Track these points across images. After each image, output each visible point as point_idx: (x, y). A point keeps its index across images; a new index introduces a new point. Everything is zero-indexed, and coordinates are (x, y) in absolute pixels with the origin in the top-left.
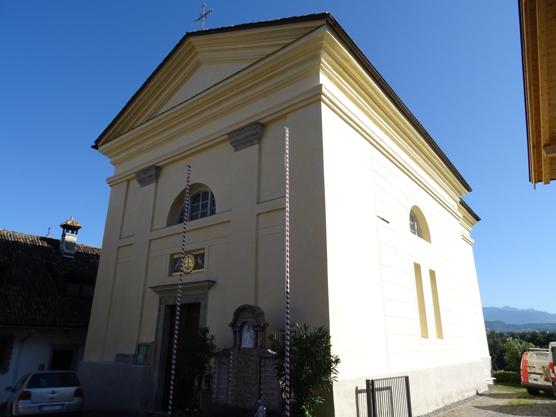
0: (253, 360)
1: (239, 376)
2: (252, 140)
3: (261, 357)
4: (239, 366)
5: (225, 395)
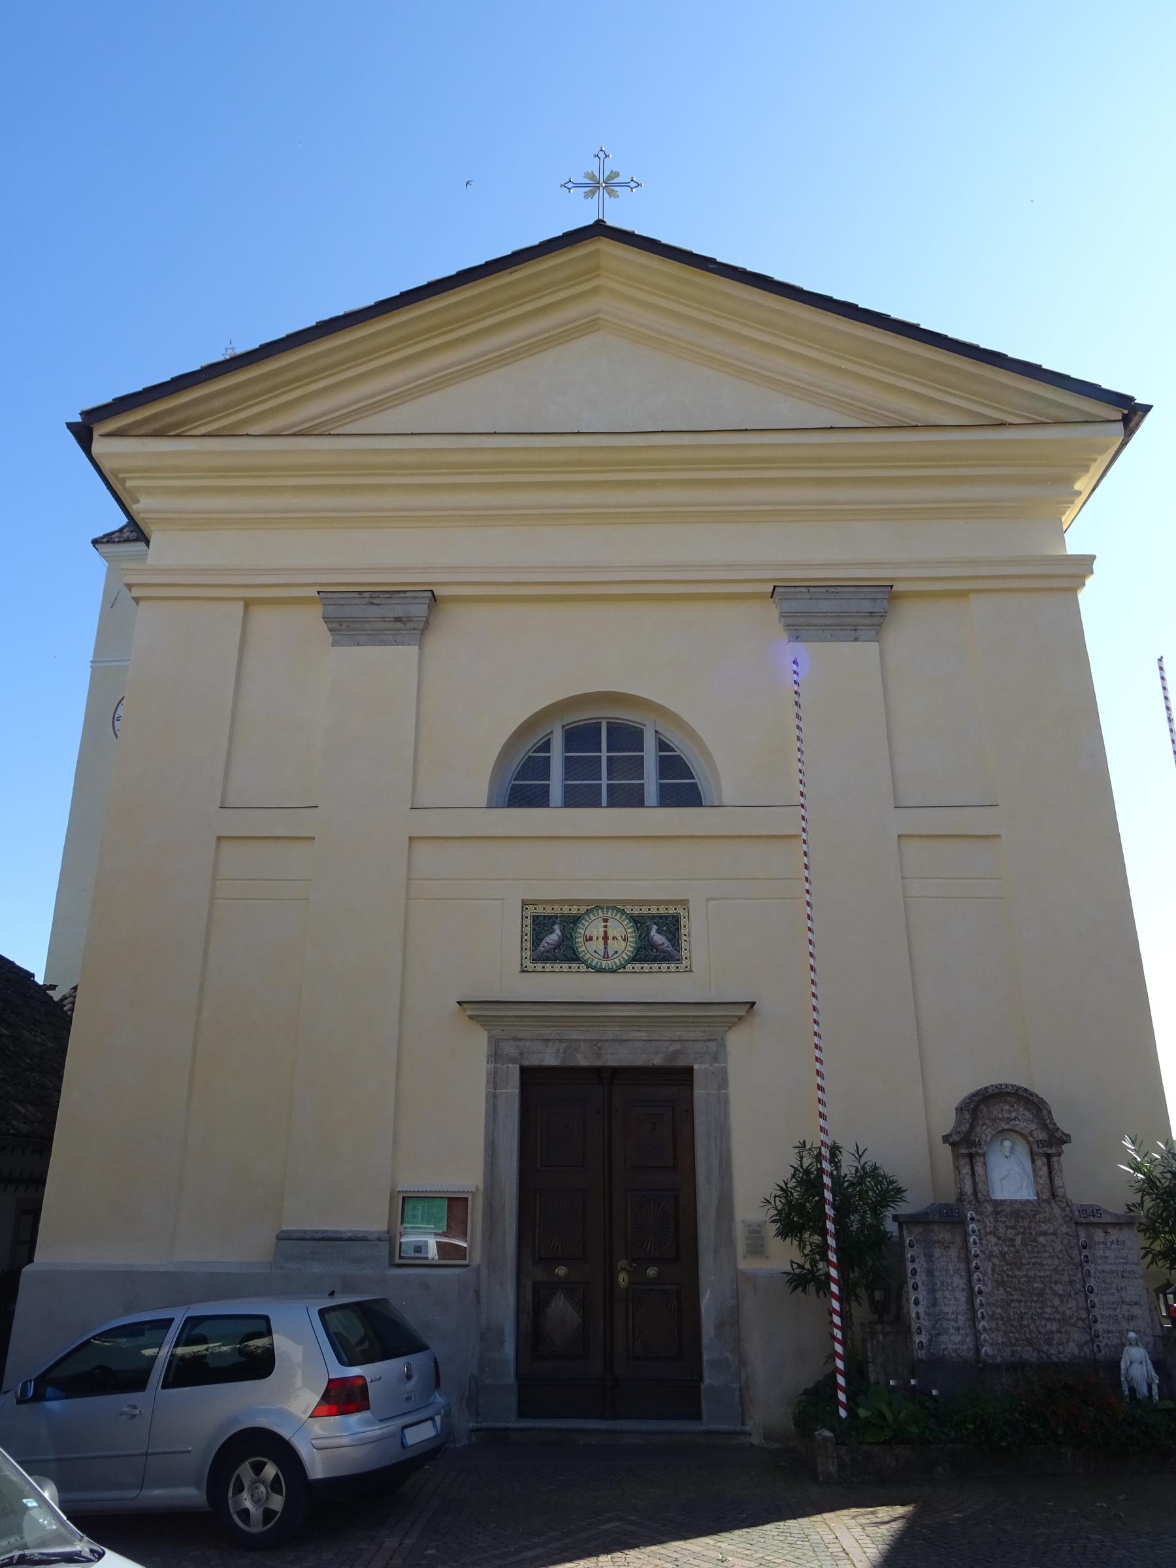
0: (1051, 1231)
1: (1008, 1276)
2: (856, 626)
3: (1077, 1224)
5: (962, 1332)
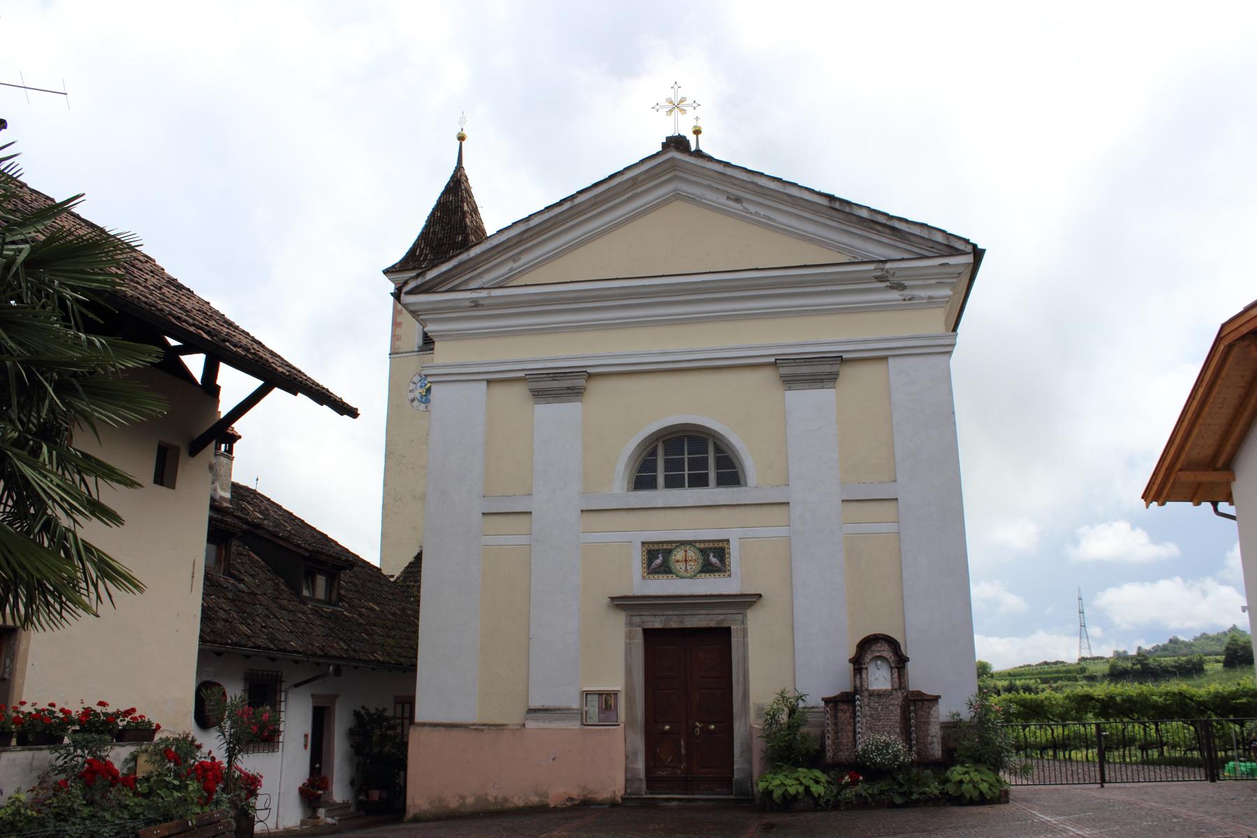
4: (873, 712)
